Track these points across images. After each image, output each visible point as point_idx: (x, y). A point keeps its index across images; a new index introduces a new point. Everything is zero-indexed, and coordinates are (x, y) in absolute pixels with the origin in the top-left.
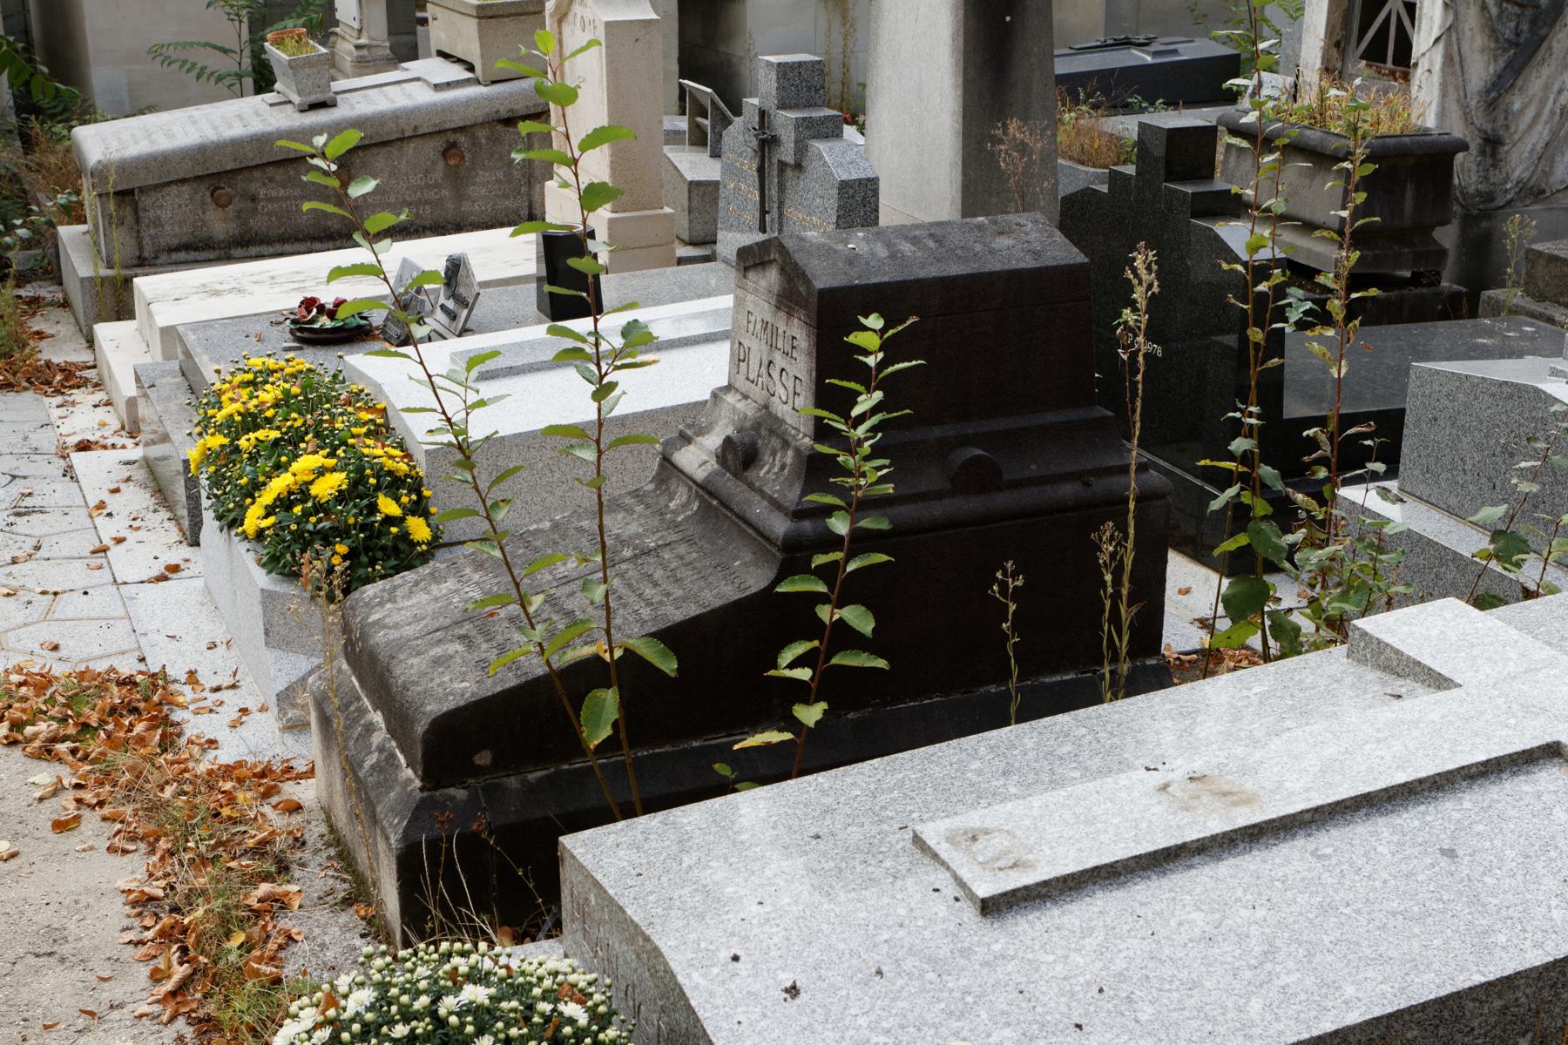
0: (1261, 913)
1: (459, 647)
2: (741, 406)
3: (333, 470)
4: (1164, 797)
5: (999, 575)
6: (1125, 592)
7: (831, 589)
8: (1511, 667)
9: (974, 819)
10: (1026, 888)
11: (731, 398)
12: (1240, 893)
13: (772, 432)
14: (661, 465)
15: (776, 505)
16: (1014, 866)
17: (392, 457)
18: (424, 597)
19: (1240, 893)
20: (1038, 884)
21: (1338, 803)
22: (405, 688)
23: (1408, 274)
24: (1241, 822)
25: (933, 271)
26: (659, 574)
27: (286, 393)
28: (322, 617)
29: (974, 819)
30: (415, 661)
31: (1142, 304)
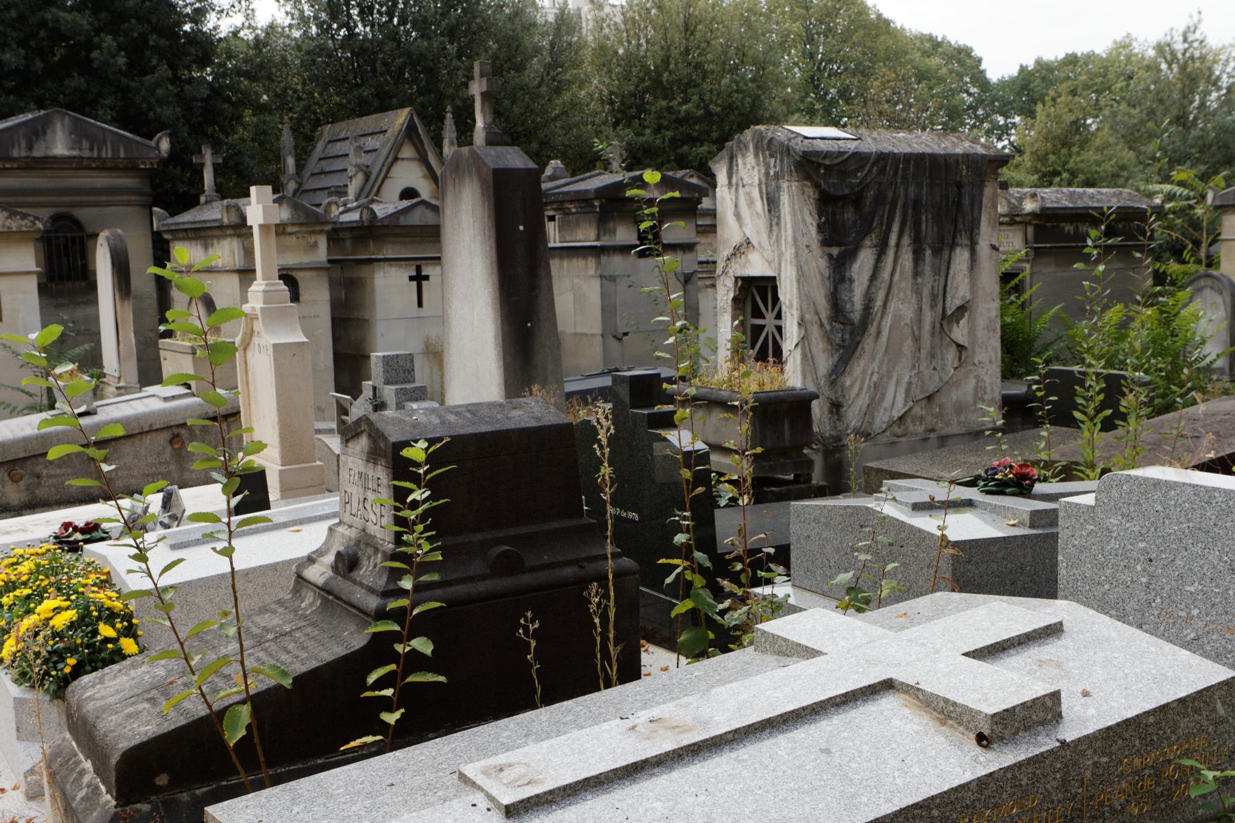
0: (701, 798)
1: (146, 705)
2: (348, 532)
3: (67, 608)
4: (633, 733)
5: (522, 621)
6: (611, 636)
7: (403, 628)
8: (858, 641)
9: (502, 759)
10: (537, 796)
11: (340, 529)
12: (686, 788)
13: (367, 544)
14: (296, 581)
15: (371, 590)
16: (529, 783)
17: (110, 598)
18: (124, 678)
19: (686, 788)
20: (545, 793)
21: (750, 726)
22: (105, 735)
23: (791, 477)
24: (685, 743)
25: (470, 430)
26: (291, 646)
27: (38, 565)
28: (53, 713)
29: (502, 759)
30: (114, 718)
31: (604, 442)
